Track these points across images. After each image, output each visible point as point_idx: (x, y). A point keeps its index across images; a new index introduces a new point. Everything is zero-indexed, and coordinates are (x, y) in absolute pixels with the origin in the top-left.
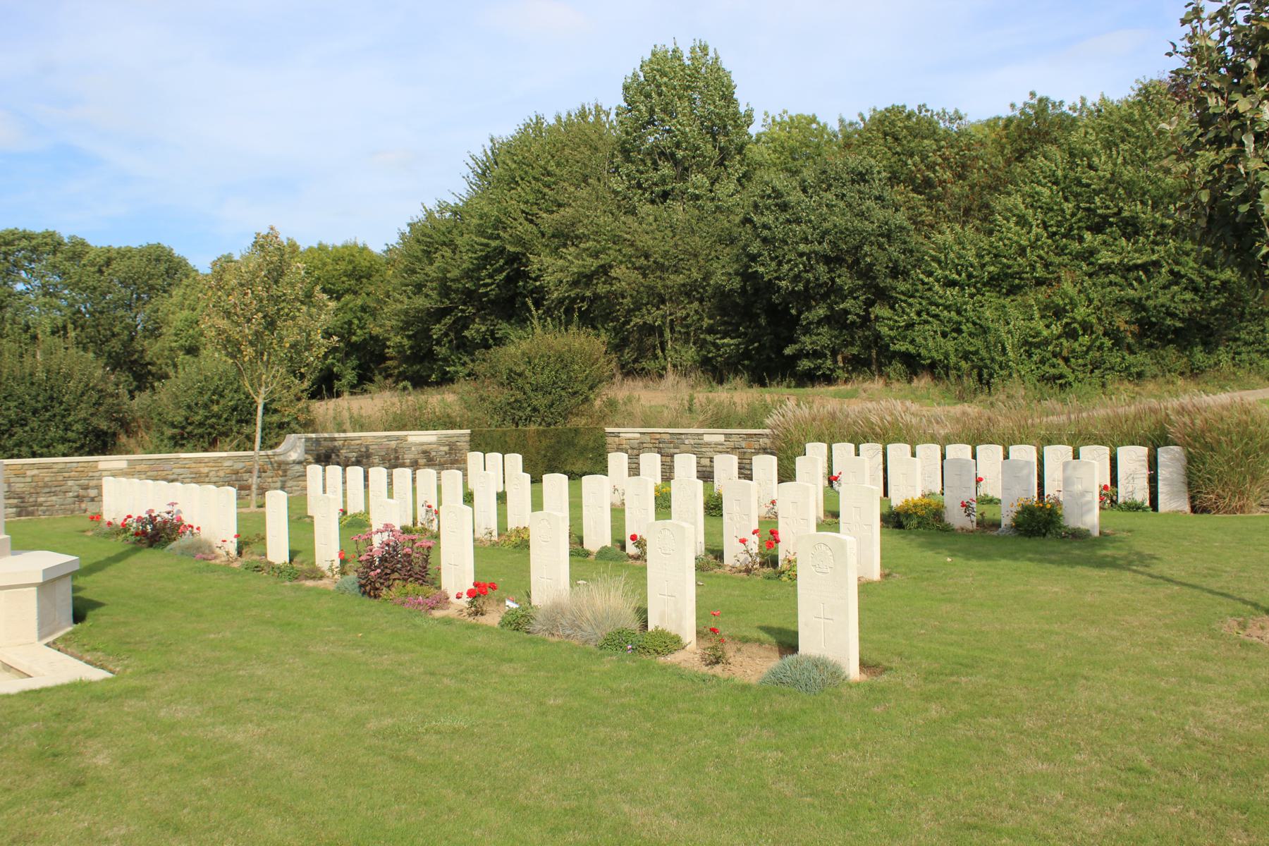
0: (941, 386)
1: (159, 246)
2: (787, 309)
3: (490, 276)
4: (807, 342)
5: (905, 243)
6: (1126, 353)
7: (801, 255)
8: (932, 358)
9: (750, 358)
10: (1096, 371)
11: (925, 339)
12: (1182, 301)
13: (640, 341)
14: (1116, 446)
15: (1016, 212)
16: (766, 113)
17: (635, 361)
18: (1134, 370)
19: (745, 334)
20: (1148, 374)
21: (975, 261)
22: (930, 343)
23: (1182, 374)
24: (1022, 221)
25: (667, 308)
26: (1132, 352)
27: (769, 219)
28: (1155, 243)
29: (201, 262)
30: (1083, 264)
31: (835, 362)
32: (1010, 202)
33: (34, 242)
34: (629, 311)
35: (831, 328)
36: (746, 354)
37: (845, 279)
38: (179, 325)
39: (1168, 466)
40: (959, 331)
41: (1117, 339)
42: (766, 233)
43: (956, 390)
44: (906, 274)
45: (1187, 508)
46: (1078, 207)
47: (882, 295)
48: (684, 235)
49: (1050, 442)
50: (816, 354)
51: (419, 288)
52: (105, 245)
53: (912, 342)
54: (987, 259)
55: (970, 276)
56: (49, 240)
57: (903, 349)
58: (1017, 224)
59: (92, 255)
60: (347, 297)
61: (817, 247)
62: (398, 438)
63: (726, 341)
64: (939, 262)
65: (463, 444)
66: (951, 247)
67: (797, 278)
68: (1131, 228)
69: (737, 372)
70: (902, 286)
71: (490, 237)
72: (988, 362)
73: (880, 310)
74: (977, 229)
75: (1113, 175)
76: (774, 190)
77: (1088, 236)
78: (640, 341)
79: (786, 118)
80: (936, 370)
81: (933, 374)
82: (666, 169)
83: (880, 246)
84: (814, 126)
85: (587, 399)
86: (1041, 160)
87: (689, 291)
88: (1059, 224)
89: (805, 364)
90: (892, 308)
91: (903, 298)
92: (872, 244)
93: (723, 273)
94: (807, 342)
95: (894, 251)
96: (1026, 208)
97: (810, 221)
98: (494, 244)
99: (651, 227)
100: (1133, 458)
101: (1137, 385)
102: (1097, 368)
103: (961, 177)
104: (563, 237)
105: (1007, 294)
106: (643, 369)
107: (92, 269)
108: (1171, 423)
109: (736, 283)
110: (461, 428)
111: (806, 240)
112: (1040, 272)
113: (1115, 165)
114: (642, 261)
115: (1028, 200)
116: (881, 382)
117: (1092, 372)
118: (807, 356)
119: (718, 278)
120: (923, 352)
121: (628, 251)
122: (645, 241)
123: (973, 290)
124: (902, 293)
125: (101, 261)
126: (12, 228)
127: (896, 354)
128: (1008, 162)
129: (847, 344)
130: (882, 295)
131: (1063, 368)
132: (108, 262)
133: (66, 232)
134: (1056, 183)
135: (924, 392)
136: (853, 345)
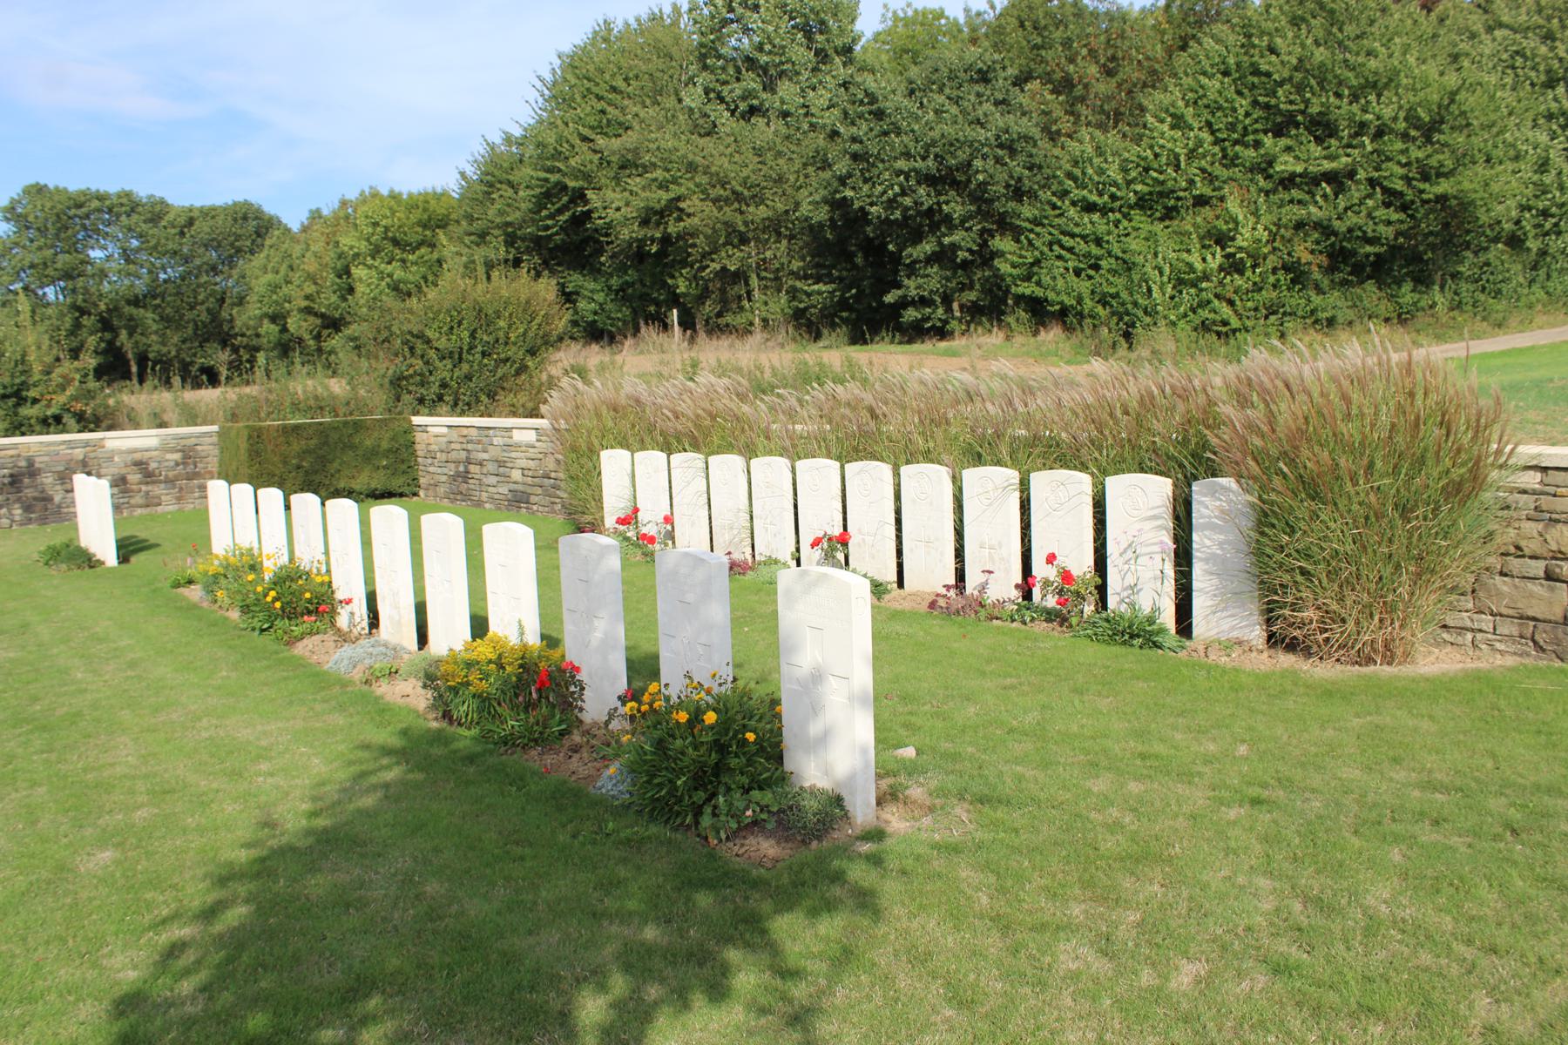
0: (1074, 340)
1: (246, 203)
2: (884, 245)
3: (551, 216)
4: (912, 287)
5: (1031, 156)
6: (1312, 293)
7: (899, 173)
8: (1062, 303)
9: (849, 308)
10: (1273, 318)
11: (1054, 278)
12: (1386, 224)
13: (723, 291)
14: (1105, 473)
15: (1172, 110)
16: (885, 6)
17: (719, 315)
18: (1323, 315)
19: (841, 279)
20: (1340, 320)
21: (1119, 178)
22: (1059, 284)
23: (1387, 320)
24: (1179, 122)
25: (751, 248)
26: (1319, 290)
27: (862, 129)
28: (1349, 146)
29: (294, 219)
30: (1260, 178)
31: (949, 310)
32: (1166, 99)
33: (108, 203)
34: (704, 256)
35: (941, 268)
36: (843, 304)
37: (956, 207)
38: (262, 290)
39: (1212, 527)
40: (1096, 267)
41: (1297, 275)
42: (856, 147)
43: (1091, 344)
44: (1032, 195)
45: (1257, 635)
46: (1255, 103)
47: (1005, 224)
48: (777, 163)
49: (978, 460)
50: (924, 302)
51: (482, 236)
52: (187, 204)
53: (1039, 284)
54: (1133, 174)
55: (1113, 197)
56: (124, 201)
57: (1028, 292)
58: (1172, 127)
59: (170, 217)
60: (423, 250)
61: (919, 164)
62: (87, 444)
63: (816, 287)
64: (1075, 179)
65: (210, 451)
66: (1090, 160)
67: (891, 204)
68: (1322, 128)
69: (833, 326)
70: (1027, 211)
71: (550, 170)
72: (1129, 306)
73: (1002, 243)
74: (1124, 136)
75: (1300, 60)
76: (867, 94)
77: (1268, 140)
78: (723, 291)
79: (910, 13)
80: (1066, 317)
81: (1064, 323)
82: (751, 82)
83: (998, 161)
84: (943, 21)
85: (523, 369)
86: (1208, 42)
87: (774, 227)
88: (1232, 127)
89: (911, 314)
90: (1018, 241)
91: (1029, 226)
92: (985, 157)
93: (811, 207)
94: (912, 287)
95: (1016, 166)
96: (1187, 106)
97: (913, 131)
98: (554, 178)
99: (735, 150)
100: (1140, 499)
101: (1327, 335)
102: (1274, 313)
103: (1110, 73)
104: (629, 165)
105: (1161, 219)
106: (727, 325)
107: (173, 231)
108: (1215, 423)
109: (822, 215)
110: (204, 423)
111: (907, 155)
112: (1201, 188)
113: (1303, 46)
114: (719, 191)
115: (1190, 95)
116: (1001, 335)
117: (1266, 317)
118: (913, 303)
119: (805, 209)
120: (1051, 296)
121: (704, 180)
122: (722, 164)
123: (1118, 216)
124: (1028, 220)
125: (182, 220)
126: (83, 187)
127: (1020, 299)
128: (1169, 52)
129: (963, 288)
130: (1005, 224)
131: (1226, 311)
132: (191, 222)
133: (144, 189)
134: (1226, 73)
135: (1052, 347)
136: (971, 288)
